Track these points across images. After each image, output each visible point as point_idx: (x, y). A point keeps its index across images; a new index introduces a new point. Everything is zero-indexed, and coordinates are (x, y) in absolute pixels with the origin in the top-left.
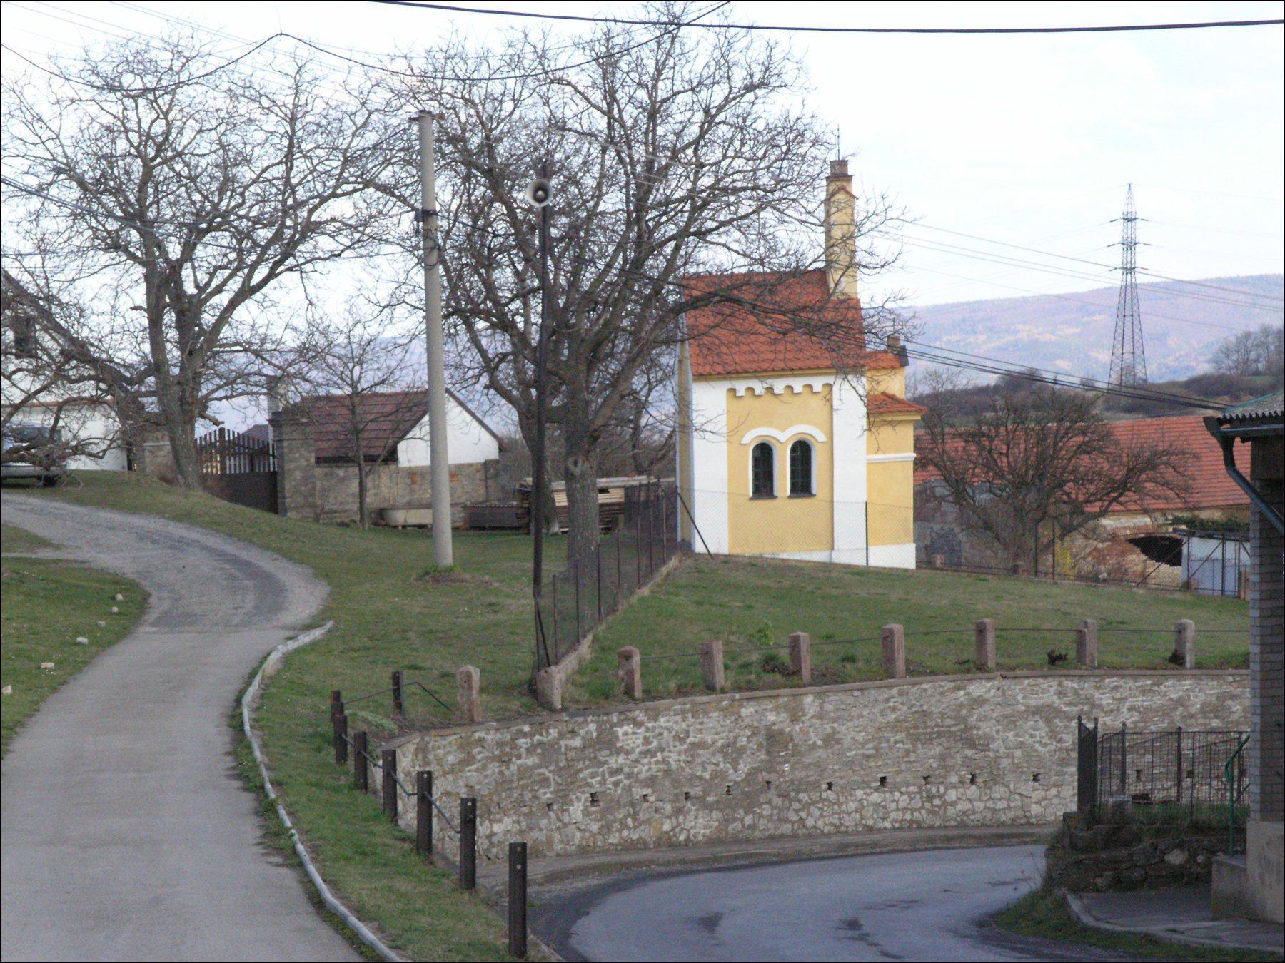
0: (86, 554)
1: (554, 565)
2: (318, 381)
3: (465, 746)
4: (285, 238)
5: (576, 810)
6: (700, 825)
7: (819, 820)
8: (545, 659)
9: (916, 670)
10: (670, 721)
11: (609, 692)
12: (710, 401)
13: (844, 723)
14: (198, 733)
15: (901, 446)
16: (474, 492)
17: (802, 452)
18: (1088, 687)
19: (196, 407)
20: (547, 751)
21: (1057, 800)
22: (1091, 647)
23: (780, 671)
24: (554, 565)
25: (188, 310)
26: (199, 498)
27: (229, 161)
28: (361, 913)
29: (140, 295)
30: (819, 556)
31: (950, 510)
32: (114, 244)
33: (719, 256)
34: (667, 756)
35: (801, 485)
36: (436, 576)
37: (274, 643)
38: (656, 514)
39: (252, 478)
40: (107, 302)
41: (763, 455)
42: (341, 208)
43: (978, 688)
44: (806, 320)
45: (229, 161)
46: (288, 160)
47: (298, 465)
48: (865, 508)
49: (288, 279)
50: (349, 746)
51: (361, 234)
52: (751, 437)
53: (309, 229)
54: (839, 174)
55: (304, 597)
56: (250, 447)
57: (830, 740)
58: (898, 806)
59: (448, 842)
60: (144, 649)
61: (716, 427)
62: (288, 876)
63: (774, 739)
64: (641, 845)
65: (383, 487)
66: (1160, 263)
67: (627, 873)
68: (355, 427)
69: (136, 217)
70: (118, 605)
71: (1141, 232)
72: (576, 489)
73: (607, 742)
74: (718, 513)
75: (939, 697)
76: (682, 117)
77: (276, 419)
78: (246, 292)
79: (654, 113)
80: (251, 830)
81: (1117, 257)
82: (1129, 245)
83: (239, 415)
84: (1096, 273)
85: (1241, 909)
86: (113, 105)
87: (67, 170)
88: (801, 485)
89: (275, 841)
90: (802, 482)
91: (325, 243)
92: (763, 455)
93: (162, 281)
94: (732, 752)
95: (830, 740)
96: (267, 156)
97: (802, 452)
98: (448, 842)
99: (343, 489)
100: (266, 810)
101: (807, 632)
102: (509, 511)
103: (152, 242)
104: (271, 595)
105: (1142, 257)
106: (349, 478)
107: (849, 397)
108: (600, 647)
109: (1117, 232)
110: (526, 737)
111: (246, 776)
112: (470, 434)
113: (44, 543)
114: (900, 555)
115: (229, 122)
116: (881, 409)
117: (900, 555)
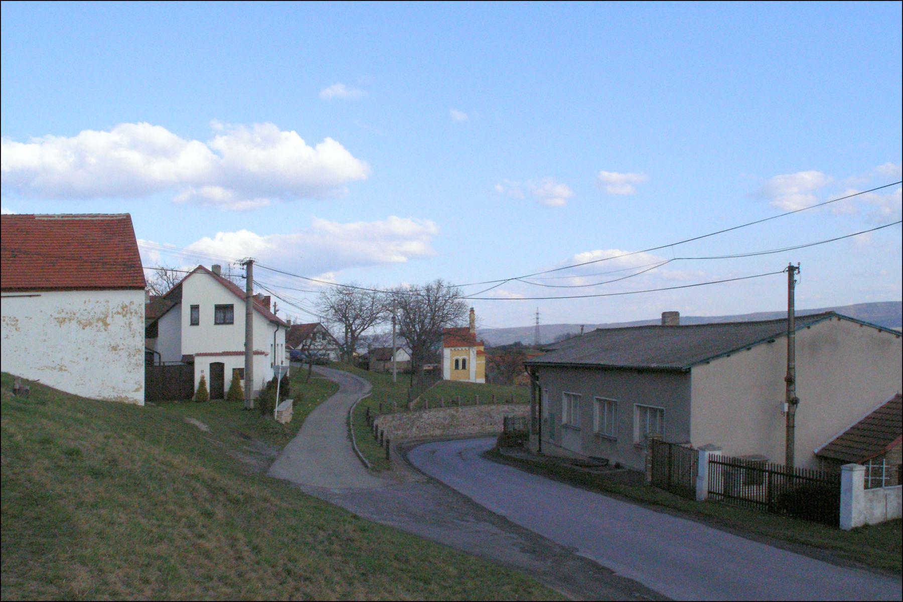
0: (330, 378)
1: (415, 382)
2: (377, 345)
3: (393, 417)
4: (372, 319)
5: (414, 430)
6: (438, 432)
7: (461, 432)
8: (410, 401)
9: (481, 403)
10: (433, 413)
11: (421, 408)
12: (447, 352)
13: (467, 414)
14: (342, 415)
15: (483, 361)
16: (404, 366)
17: (464, 361)
18: (513, 407)
19: (354, 350)
20: (409, 419)
21: (500, 428)
22: (515, 400)
23: (454, 403)
24: (415, 382)
25: (353, 332)
26: (353, 368)
27: (362, 305)
28: (361, 451)
29: (344, 330)
30: (467, 381)
31: (496, 371)
32: (340, 320)
33: (449, 325)
34: (433, 419)
35: (464, 367)
36: (393, 384)
37: (359, 397)
38: (437, 372)
39: (364, 364)
40: (338, 330)
41: (457, 361)
42: (381, 314)
43: (493, 407)
44: (465, 337)
45: (362, 305)
46: (372, 306)
47: (372, 360)
48: (476, 371)
49: (371, 327)
50: (369, 418)
51: (385, 319)
52: (455, 358)
53: (376, 318)
54: (472, 310)
55: (368, 387)
56: (364, 357)
57: (464, 416)
58: (477, 429)
59: (379, 437)
60: (338, 396)
61: (448, 356)
62: (350, 443)
63: (453, 416)
64: (426, 436)
65: (388, 365)
66: (542, 322)
67: (422, 441)
68: (385, 355)
69: (344, 316)
70: (334, 388)
71: (540, 316)
72: (424, 367)
73: (421, 417)
74: (448, 373)
75: (485, 408)
76: (441, 301)
77: (369, 352)
78: (363, 329)
79: (436, 300)
80: (346, 434)
81: (535, 321)
82: (537, 318)
83: (362, 351)
84: (532, 323)
85: (528, 451)
86: (341, 296)
87: (332, 307)
88: (464, 367)
89: (350, 437)
90: (465, 367)
91: (378, 321)
92: (457, 361)
93: (349, 326)
94: (445, 419)
95: (464, 416)
96: (368, 305)
97: (464, 361)
98: (379, 437)
99: (381, 366)
100: (349, 431)
101: (464, 395)
102: (410, 371)
103: (347, 319)
104: (362, 386)
105: (540, 321)
106: (382, 363)
107: (473, 351)
108: (421, 398)
109: (535, 316)
110: (405, 415)
111: (348, 424)
112: (403, 356)
113: (321, 375)
114: (482, 380)
115: (362, 299)
116: (479, 353)
117: (482, 380)
